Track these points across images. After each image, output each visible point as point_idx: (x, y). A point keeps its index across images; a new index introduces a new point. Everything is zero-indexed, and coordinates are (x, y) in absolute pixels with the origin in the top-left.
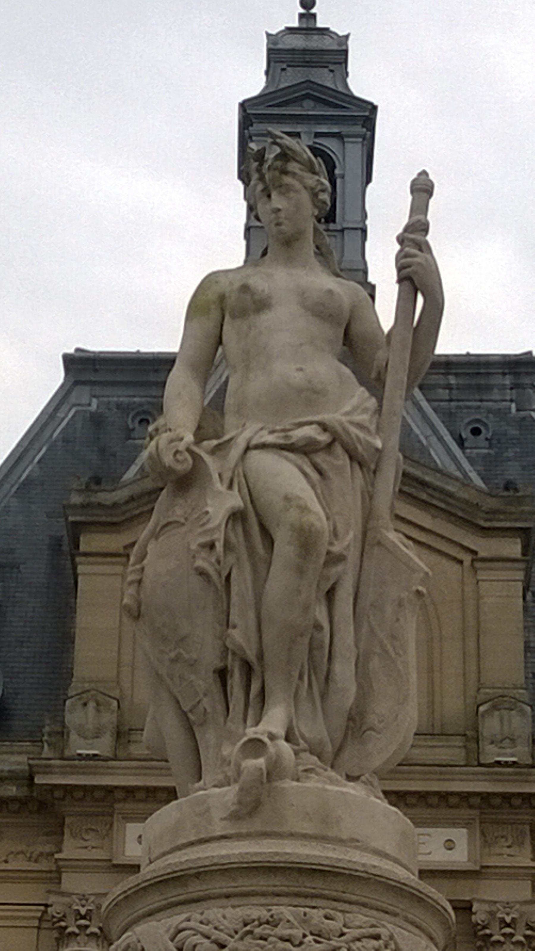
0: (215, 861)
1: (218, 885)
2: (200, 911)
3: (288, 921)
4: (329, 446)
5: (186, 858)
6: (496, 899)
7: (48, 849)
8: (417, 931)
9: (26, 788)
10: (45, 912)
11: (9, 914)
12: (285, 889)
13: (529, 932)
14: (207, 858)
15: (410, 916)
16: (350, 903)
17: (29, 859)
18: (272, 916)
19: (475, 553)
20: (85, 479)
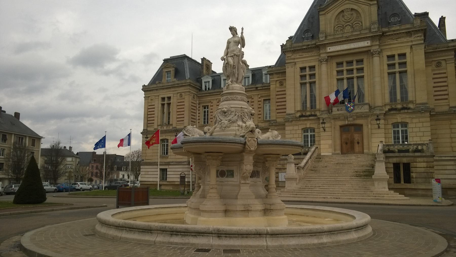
4: (234, 55)
7: (319, 52)
19: (370, 4)
20: (319, 5)
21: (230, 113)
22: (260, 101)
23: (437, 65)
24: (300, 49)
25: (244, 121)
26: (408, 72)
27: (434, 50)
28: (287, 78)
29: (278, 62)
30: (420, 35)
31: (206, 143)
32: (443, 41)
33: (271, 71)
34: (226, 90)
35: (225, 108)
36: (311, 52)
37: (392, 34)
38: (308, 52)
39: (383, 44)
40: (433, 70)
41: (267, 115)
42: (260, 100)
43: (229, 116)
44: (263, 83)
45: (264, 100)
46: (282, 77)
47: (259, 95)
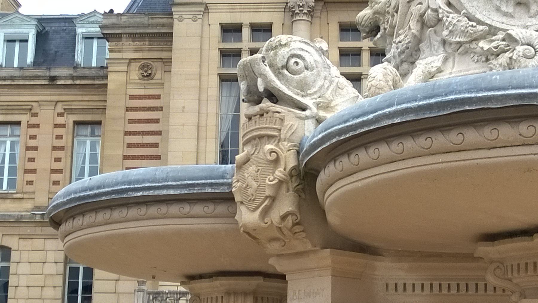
11: (274, 7)
13: (309, 9)
22: (63, 126)
28: (175, 55)
42: (61, 120)
44: (77, 64)
45: (77, 123)
46: (150, 50)
47: (60, 105)
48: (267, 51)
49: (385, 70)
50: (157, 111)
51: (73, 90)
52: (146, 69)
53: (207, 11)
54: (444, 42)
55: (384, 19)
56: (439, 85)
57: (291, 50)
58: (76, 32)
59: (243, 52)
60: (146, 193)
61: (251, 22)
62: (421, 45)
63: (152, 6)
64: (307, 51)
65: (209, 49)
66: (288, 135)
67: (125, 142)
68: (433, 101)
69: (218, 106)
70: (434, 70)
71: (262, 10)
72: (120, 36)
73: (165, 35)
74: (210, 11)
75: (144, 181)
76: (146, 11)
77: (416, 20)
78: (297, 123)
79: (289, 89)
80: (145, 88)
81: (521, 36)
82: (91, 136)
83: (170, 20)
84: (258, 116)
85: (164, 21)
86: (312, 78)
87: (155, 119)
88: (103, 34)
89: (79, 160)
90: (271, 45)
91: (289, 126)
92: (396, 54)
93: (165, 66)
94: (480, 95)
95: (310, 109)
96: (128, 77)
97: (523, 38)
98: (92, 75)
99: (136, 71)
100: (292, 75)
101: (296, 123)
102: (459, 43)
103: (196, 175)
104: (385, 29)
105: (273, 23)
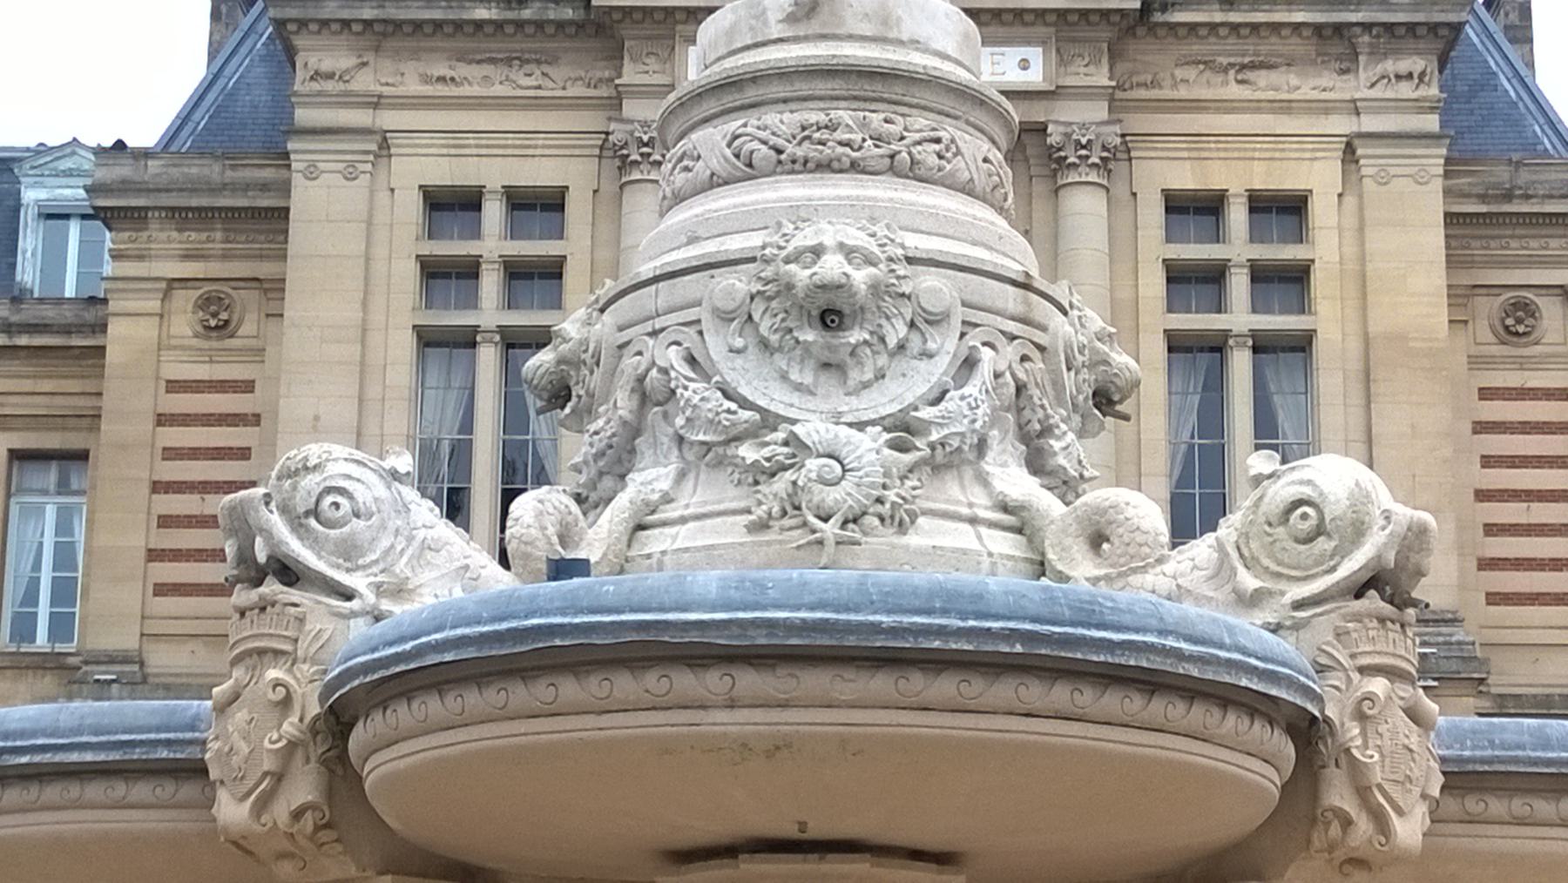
0: (772, 64)
1: (774, 90)
2: (757, 116)
3: (847, 125)
5: (741, 62)
6: (1071, 120)
7: (607, 74)
8: (979, 135)
9: (582, 11)
10: (606, 140)
12: (844, 93)
13: (1105, 154)
14: (763, 62)
15: (972, 119)
16: (911, 106)
17: (589, 86)
18: (830, 120)
21: (903, 330)
23: (1510, 321)
24: (438, 25)
25: (1061, 460)
26: (1320, 347)
27: (1494, 208)
28: (297, 273)
29: (197, 116)
30: (1416, 64)
31: (975, 688)
32: (1549, 146)
33: (124, 187)
34: (776, 31)
35: (848, 252)
36: (538, 62)
37: (1213, 27)
38: (508, 62)
39: (1142, 93)
40: (1477, 362)
41: (31, 597)
43: (880, 376)
44: (23, 291)
46: (226, 256)
48: (279, 478)
49: (540, 506)
50: (245, 425)
51: (7, 362)
52: (213, 308)
53: (385, 152)
54: (680, 440)
55: (578, 376)
56: (519, 597)
57: (325, 479)
58: (19, 199)
59: (484, 266)
60: (37, 758)
61: (507, 184)
62: (637, 441)
63: (233, 133)
64: (358, 480)
65: (390, 258)
66: (312, 650)
67: (153, 511)
68: (504, 626)
69: (412, 420)
70: (655, 497)
71: (538, 152)
72: (143, 214)
73: (269, 215)
74: (393, 151)
75: (34, 734)
76: (216, 145)
77: (629, 388)
78: (331, 627)
79: (320, 557)
80: (211, 362)
81: (816, 438)
82: (59, 494)
83: (283, 173)
84: (257, 611)
85: (268, 174)
86: (368, 535)
87: (239, 449)
88: (94, 208)
89: (25, 557)
90: (289, 468)
91: (313, 633)
92: (590, 458)
93: (268, 299)
94: (577, 620)
95: (361, 596)
96: (165, 328)
97: (820, 443)
98: (63, 322)
99: (185, 312)
100: (327, 531)
101: (330, 626)
102: (703, 443)
103: (141, 723)
104: (579, 397)
105: (567, 187)
